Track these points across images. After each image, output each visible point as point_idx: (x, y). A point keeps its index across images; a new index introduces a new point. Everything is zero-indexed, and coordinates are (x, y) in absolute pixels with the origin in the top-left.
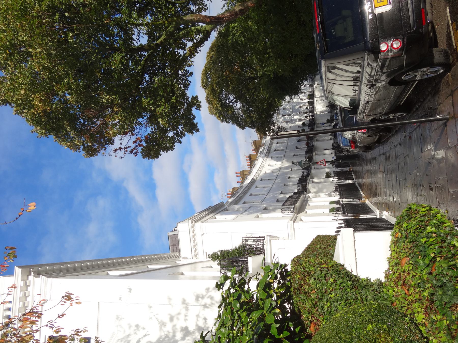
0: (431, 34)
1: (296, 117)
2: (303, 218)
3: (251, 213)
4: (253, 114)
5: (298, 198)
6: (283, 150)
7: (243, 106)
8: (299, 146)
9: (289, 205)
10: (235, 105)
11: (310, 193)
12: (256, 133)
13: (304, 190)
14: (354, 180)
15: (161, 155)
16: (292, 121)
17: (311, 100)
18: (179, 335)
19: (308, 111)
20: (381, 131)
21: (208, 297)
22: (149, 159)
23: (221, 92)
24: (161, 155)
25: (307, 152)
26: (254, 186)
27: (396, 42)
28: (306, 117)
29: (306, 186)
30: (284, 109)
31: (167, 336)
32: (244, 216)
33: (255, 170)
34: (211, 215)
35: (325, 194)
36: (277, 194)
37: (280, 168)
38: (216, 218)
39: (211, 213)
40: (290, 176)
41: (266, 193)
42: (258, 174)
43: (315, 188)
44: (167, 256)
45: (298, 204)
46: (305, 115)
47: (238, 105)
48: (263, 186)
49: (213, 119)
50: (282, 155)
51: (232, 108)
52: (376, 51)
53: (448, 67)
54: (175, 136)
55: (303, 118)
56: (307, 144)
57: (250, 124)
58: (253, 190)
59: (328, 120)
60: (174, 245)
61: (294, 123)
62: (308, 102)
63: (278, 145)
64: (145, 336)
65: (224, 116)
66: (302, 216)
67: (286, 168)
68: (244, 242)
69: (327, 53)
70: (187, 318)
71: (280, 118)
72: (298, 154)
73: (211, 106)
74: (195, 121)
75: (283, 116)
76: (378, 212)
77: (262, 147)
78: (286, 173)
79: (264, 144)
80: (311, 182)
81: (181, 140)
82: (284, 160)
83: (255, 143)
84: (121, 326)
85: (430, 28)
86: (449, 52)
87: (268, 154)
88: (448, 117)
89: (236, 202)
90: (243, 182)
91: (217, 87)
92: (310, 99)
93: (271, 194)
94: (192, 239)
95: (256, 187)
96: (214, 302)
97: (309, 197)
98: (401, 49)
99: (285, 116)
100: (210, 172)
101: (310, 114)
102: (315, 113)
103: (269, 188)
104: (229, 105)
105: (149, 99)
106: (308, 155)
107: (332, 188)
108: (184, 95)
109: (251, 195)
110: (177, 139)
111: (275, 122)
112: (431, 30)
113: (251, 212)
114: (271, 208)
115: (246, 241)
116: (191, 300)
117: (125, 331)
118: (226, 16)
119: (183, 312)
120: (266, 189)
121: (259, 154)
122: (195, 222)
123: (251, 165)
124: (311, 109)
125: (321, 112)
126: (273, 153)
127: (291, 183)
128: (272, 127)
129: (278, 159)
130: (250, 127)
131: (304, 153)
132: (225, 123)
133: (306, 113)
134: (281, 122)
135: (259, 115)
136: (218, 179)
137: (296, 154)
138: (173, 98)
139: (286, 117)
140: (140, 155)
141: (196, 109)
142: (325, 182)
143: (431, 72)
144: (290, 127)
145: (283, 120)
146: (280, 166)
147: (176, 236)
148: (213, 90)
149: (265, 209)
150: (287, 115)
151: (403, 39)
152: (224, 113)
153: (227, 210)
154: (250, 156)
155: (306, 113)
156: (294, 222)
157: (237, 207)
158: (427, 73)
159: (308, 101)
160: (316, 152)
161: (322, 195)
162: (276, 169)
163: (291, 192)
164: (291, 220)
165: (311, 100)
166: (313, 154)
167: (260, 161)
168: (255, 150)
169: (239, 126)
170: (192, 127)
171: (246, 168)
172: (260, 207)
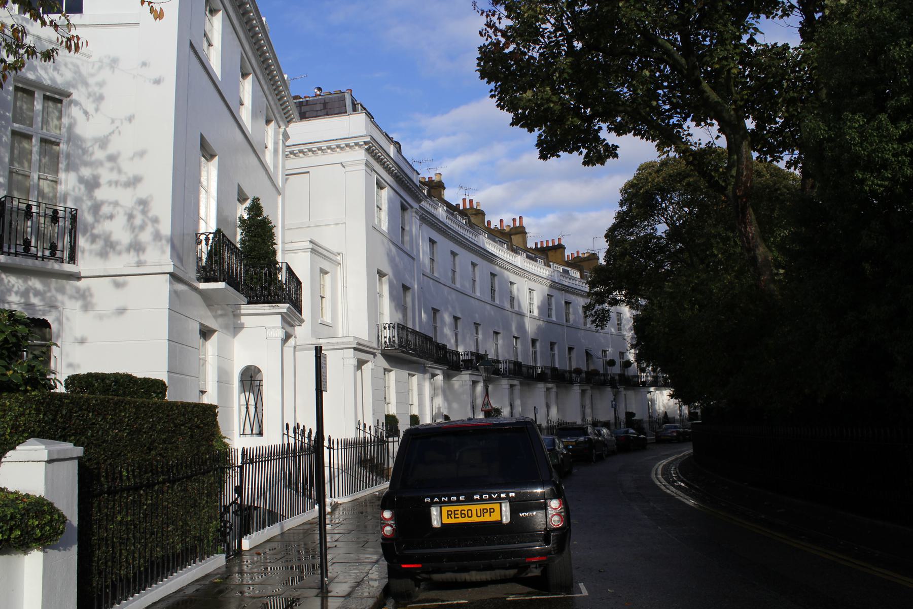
2: (367, 368)
3: (392, 260)
8: (574, 354)
15: (489, 82)
18: (86, 172)
21: (144, 221)
22: (478, 59)
24: (489, 82)
25: (554, 370)
26: (477, 260)
31: (85, 151)
32: (383, 248)
33: (519, 260)
37: (521, 315)
39: (396, 177)
40: (499, 336)
41: (458, 285)
42: (508, 266)
44: (285, 102)
48: (477, 279)
50: (554, 318)
56: (578, 371)
58: (465, 257)
59: (633, 414)
64: (86, 113)
67: (521, 327)
70: (113, 186)
72: (556, 352)
73: (656, 168)
77: (578, 275)
78: (507, 327)
80: (475, 378)
82: (541, 323)
84: (100, 68)
87: (555, 286)
96: (137, 230)
102: (652, 389)
103: (470, 292)
105: (570, 71)
113: (397, 259)
116: (142, 191)
117: (93, 75)
118: (748, 229)
119: (123, 178)
120: (468, 284)
122: (367, 150)
125: (653, 401)
126: (561, 297)
129: (546, 308)
140: (483, 41)
147: (342, 111)
149: (405, 288)
153: (404, 208)
156: (355, 349)
160: (554, 390)
162: (519, 306)
166: (549, 382)
167: (539, 269)
168: (578, 257)
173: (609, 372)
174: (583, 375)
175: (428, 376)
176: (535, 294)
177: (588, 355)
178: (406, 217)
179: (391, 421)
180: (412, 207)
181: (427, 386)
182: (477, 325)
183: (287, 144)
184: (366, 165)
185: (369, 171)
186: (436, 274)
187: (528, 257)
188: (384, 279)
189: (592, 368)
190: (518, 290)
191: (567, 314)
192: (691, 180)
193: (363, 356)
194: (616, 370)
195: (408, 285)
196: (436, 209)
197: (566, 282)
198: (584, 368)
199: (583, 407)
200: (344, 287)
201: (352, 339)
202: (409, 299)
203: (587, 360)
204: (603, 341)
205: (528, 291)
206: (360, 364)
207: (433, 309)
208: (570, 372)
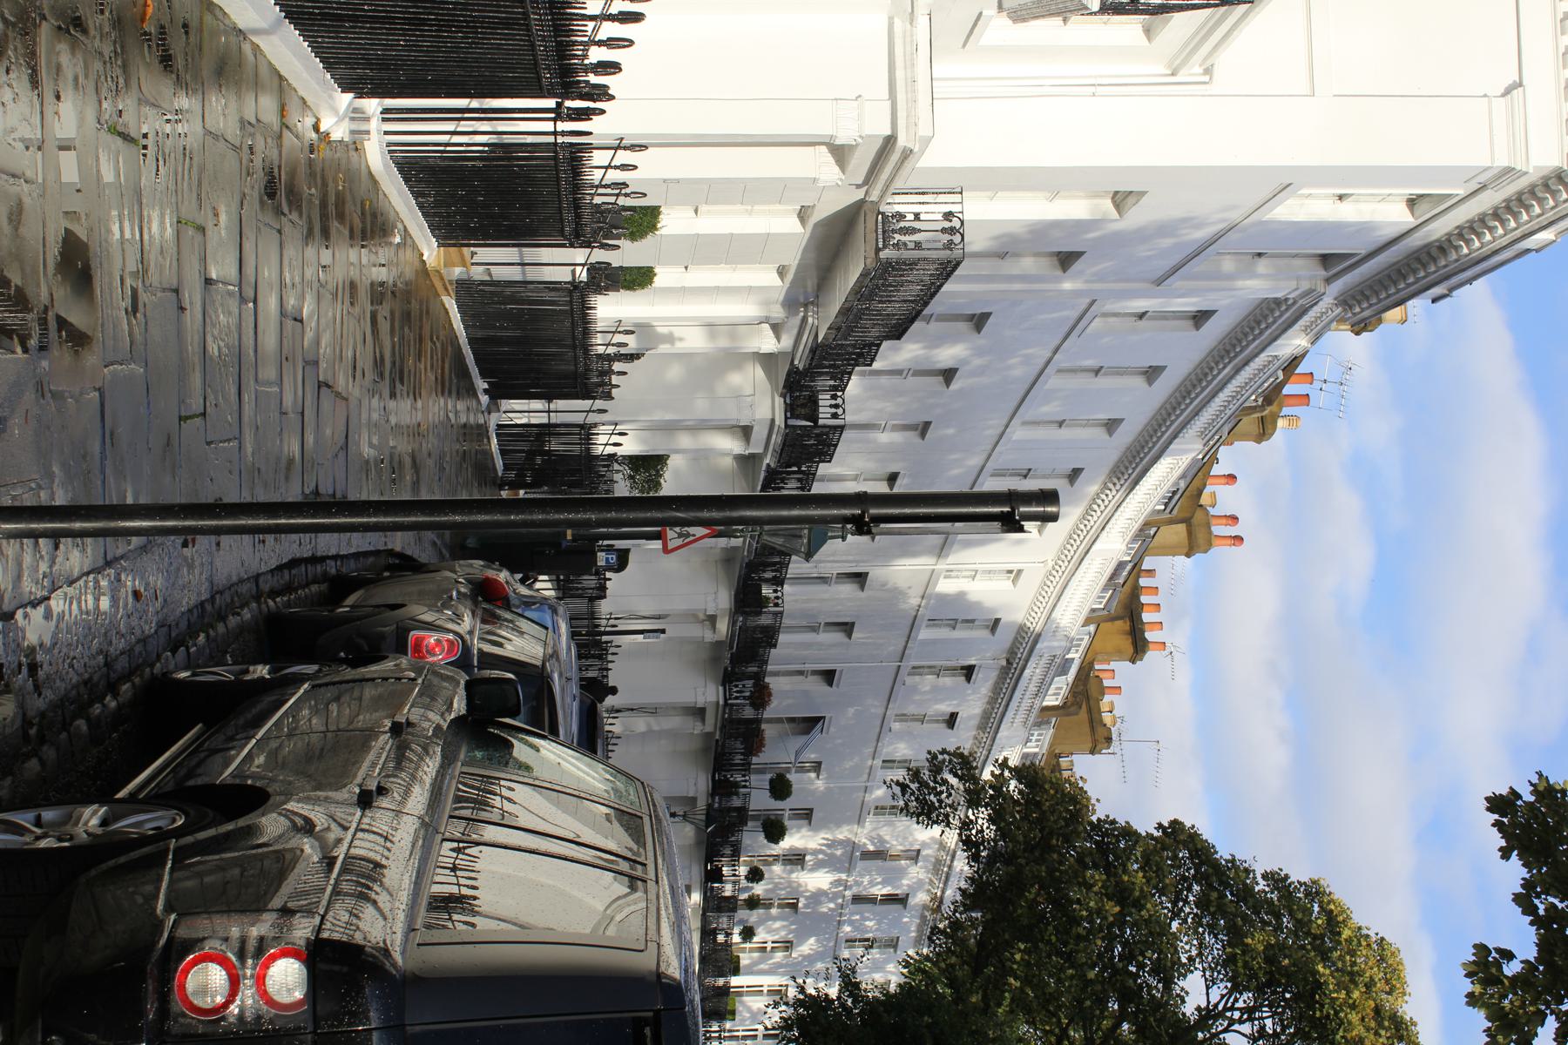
1: (816, 880)
2: (828, 171)
3: (1164, 229)
4: (1099, 911)
5: (850, 316)
6: (916, 670)
7: (1168, 971)
8: (816, 686)
9: (913, 264)
11: (767, 360)
12: (1092, 790)
13: (807, 380)
14: (494, 420)
16: (852, 857)
17: (721, 982)
19: (742, 914)
20: (322, 625)
25: (769, 637)
26: (1126, 435)
27: (207, 1002)
28: (755, 875)
29: (791, 410)
30: (893, 944)
32: (1211, 210)
33: (1114, 545)
34: (1439, 229)
35: (680, 347)
36: (981, 371)
38: (1412, 202)
39: (1442, 247)
41: (1052, 381)
42: (1096, 519)
43: (738, 396)
46: (759, 889)
47: (1195, 992)
48: (1065, 433)
50: (924, 634)
52: (334, 964)
55: (777, 869)
56: (761, 696)
57: (1129, 851)
58: (1138, 404)
61: (833, 844)
62: (736, 971)
63: (946, 708)
66: (834, 189)
69: (646, 1021)
71: (920, 883)
73: (1388, 1002)
74: (1515, 872)
75: (899, 900)
76: (375, 156)
77: (1051, 701)
80: (759, 434)
82: (915, 601)
83: (1099, 738)
87: (1020, 649)
89: (1267, 319)
90: (1199, 473)
92: (725, 991)
93: (1019, 370)
95: (1111, 425)
97: (776, 329)
98: (180, 951)
99: (891, 899)
100: (1398, 607)
101: (728, 890)
103: (1026, 412)
106: (765, 620)
107: (629, 384)
113: (1167, 242)
114: (1028, 264)
120: (1050, 410)
121: (1076, 656)
123: (1136, 591)
124: (724, 921)
126: (987, 654)
127: (884, 438)
128: (981, 817)
129: (957, 615)
130: (1128, 832)
131: (783, 638)
132: (1298, 874)
133: (753, 903)
134: (915, 856)
135: (1061, 904)
136: (1350, 556)
137: (838, 637)
139: (880, 891)
141: (1508, 955)
142: (670, 428)
144: (860, 821)
145: (902, 872)
146: (942, 566)
149: (1066, 260)
150: (871, 900)
151: (164, 1012)
153: (1326, 260)
154: (1138, 646)
155: (753, 903)
156: (890, 141)
157: (1258, 286)
158: (38, 831)
159: (735, 981)
160: (709, 636)
161: (694, 341)
163: (884, 380)
164: (907, 154)
165: (721, 982)
166: (733, 623)
167: (1075, 607)
168: (1102, 691)
169: (1199, 849)
171: (1171, 573)
172: (1101, 277)
173: (754, 779)
174: (749, 713)
177: (809, 724)
178: (1298, 262)
180: (1328, 281)
181: (746, 309)
182: (924, 429)
184: (1508, 171)
185: (1483, 178)
188: (1108, 204)
189: (769, 731)
193: (860, 163)
194: (760, 799)
195: (1078, 266)
196: (1306, 330)
197: (1033, 671)
198: (772, 710)
199: (653, 711)
201: (924, 131)
204: (848, 764)
205: (1015, 567)
206: (840, 153)
208: (759, 678)
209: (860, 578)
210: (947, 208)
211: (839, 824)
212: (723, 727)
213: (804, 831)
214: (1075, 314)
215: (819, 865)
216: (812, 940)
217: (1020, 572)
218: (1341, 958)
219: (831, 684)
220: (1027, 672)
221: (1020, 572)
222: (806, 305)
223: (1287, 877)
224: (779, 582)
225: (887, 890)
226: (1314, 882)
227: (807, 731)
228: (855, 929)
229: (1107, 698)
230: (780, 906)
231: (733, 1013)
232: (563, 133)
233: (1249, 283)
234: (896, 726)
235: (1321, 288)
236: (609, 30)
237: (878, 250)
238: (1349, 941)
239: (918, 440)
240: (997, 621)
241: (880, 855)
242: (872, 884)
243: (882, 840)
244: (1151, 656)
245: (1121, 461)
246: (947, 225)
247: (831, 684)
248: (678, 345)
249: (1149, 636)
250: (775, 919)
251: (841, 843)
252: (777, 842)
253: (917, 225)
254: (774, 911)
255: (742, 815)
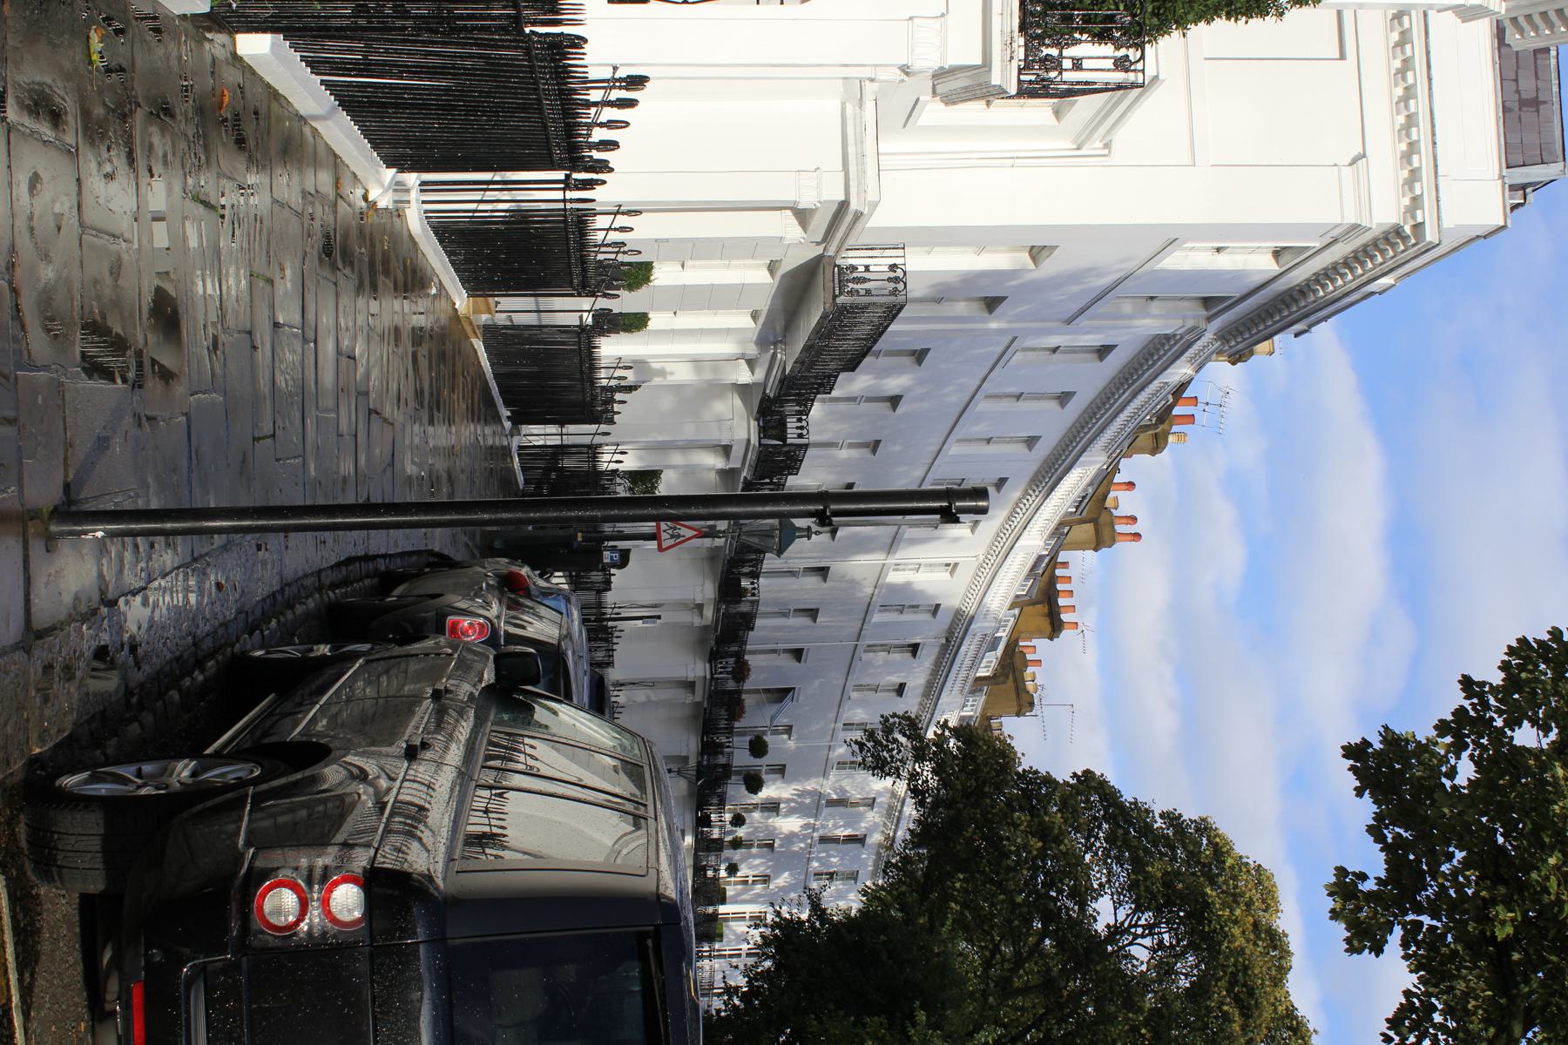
0: (107, 956)
1: (789, 824)
3: (1073, 277)
4: (1025, 847)
5: (812, 352)
6: (871, 648)
7: (1083, 895)
8: (787, 662)
9: (865, 307)
10: (1122, 914)
11: (743, 390)
16: (818, 805)
17: (710, 910)
19: (727, 853)
20: (375, 612)
23: (1198, 991)
25: (747, 621)
26: (1043, 450)
27: (281, 921)
28: (738, 820)
29: (764, 431)
32: (1111, 261)
33: (1034, 541)
35: (671, 379)
39: (1303, 290)
41: (981, 406)
42: (1019, 520)
45: (812, 318)
46: (741, 832)
47: (1105, 912)
49: (1254, 840)
50: (877, 617)
51: (1140, 893)
52: (388, 889)
53: (38, 790)
54: (1499, 723)
55: (756, 815)
57: (1049, 796)
58: (1053, 423)
60: (1535, 103)
61: (803, 794)
62: (723, 901)
63: (896, 679)
65: (1191, 855)
68: (1133, 54)
71: (875, 825)
75: (859, 840)
77: (982, 673)
79: (973, 692)
80: (737, 452)
81: (1458, 699)
82: (869, 590)
83: (1024, 703)
85: (113, 986)
86: (28, 867)
87: (957, 628)
88: (54, 528)
90: (1104, 481)
91: (1225, 1014)
94: (1421, 133)
95: (1031, 442)
97: (751, 363)
98: (257, 878)
99: (851, 839)
100: (1267, 597)
101: (716, 834)
103: (960, 432)
104: (1158, 911)
107: (628, 410)
108: (1430, 960)
109: (1064, 398)
110: (1486, 706)
111: (910, 802)
112: (107, 975)
113: (1075, 289)
115: (1122, 64)
120: (981, 429)
121: (1003, 634)
122: (1398, 231)
123: (1053, 580)
124: (712, 859)
126: (930, 634)
127: (844, 454)
128: (926, 770)
129: (904, 601)
130: (1048, 780)
131: (759, 622)
132: (1189, 813)
133: (737, 844)
134: (871, 803)
135: (994, 842)
136: (1226, 557)
137: (804, 621)
138: (1509, 930)
139: (842, 832)
143: (123, 780)
144: (825, 775)
145: (861, 816)
147: (1514, 155)
148: (1247, 1003)
150: (835, 840)
151: (245, 928)
152: (1188, 873)
153: (1207, 302)
155: (737, 844)
156: (844, 205)
157: (1152, 324)
158: (139, 781)
159: (722, 909)
160: (697, 621)
161: (683, 374)
162: (913, 542)
163: (842, 406)
164: (858, 216)
165: (710, 910)
166: (717, 610)
167: (1011, 580)
168: (1026, 663)
169: (1108, 794)
170: (1385, 768)
171: (1081, 564)
174: (731, 685)
175: (752, 350)
176: (945, 575)
177: (782, 694)
179: (639, 274)
180: (1209, 319)
181: (727, 348)
182: (875, 446)
183: (1431, 14)
184: (1355, 227)
185: (1335, 233)
186: (1018, 357)
187: (1040, 558)
189: (748, 700)
190: (956, 540)
191: (888, 649)
192: (1236, 1027)
193: (819, 224)
194: (742, 758)
195: (1001, 309)
196: (1191, 361)
197: (968, 648)
198: (748, 685)
199: (651, 684)
200: (1014, 159)
201: (872, 196)
202: (961, 308)
203: (767, 691)
204: (814, 728)
205: (952, 561)
207: (925, 352)
208: (739, 656)
209: (823, 572)
210: (892, 261)
211: (807, 777)
212: (710, 697)
213: (779, 783)
214: (1000, 349)
215: (791, 812)
216: (786, 874)
217: (956, 565)
218: (1226, 882)
219: (799, 660)
220: (963, 649)
221: (956, 565)
222: (775, 344)
223: (1180, 815)
224: (755, 575)
225: (848, 832)
226: (1203, 820)
227: (780, 700)
228: (822, 864)
229: (1030, 670)
230: (759, 846)
231: (721, 936)
232: (571, 201)
233: (1147, 321)
234: (854, 695)
235: (1203, 325)
236: (608, 114)
237: (835, 297)
238: (1232, 868)
239: (870, 456)
240: (938, 606)
241: (842, 802)
242: (836, 826)
243: (844, 791)
244: (1066, 634)
245: (1039, 471)
246: (892, 275)
247: (799, 660)
248: (670, 378)
249: (1065, 617)
250: (755, 857)
251: (809, 793)
252: (755, 793)
253: (867, 275)
254: (754, 850)
255: (727, 771)
